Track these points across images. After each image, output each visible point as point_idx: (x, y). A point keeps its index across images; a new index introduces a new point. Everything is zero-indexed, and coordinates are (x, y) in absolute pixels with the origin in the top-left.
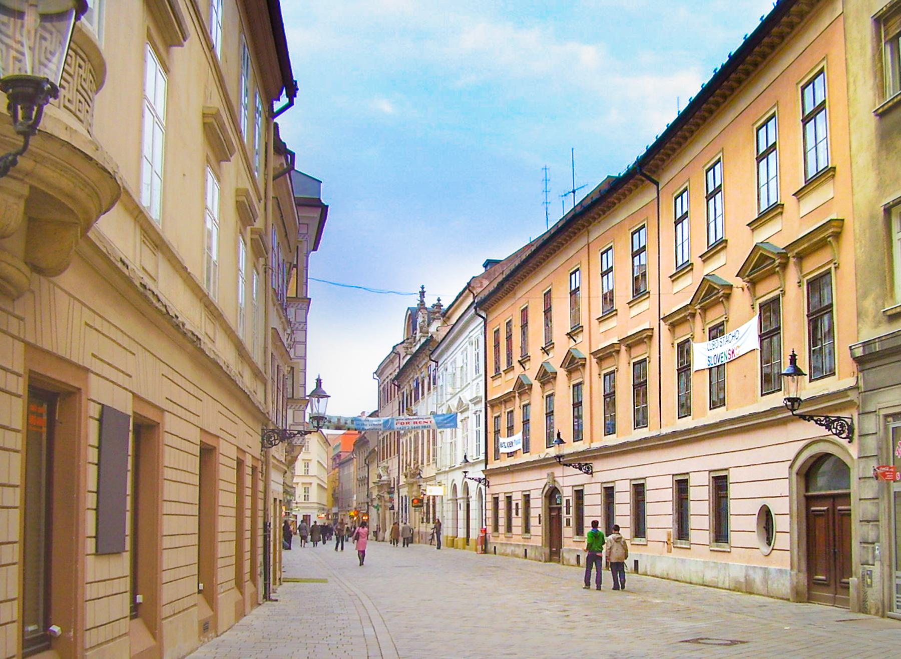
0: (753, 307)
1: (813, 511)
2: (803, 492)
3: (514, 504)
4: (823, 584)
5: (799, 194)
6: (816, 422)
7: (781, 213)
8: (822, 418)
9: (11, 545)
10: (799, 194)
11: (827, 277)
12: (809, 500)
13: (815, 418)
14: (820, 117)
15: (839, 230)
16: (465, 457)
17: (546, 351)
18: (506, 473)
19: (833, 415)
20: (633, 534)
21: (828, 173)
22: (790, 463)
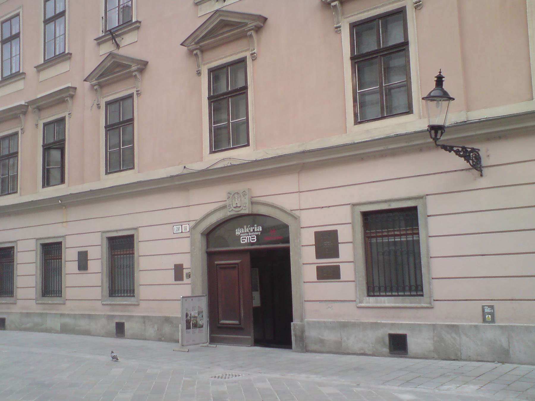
0: (99, 107)
1: (217, 265)
2: (205, 248)
3: (70, 256)
4: (235, 328)
5: (40, 68)
6: (455, 151)
7: (24, 78)
8: (460, 149)
9: (252, 217)
10: (40, 68)
11: (129, 101)
12: (211, 255)
13: (455, 149)
14: (14, 42)
15: (144, 67)
16: (440, 80)
17: (112, 35)
18: (362, 158)
19: (469, 146)
20: (107, 292)
21: (65, 57)
22: (192, 224)
